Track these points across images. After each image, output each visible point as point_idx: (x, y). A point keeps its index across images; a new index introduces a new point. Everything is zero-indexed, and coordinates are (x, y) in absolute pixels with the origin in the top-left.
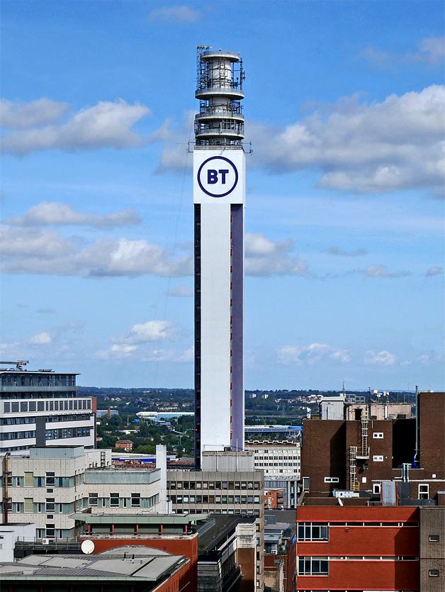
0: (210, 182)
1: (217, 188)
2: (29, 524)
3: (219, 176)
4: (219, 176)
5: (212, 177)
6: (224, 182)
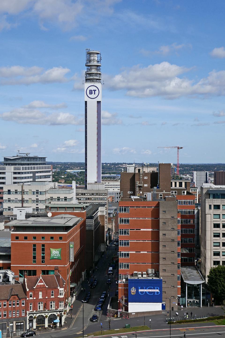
0: (90, 94)
1: (92, 96)
2: (30, 207)
3: (93, 92)
4: (93, 92)
5: (91, 92)
6: (95, 94)
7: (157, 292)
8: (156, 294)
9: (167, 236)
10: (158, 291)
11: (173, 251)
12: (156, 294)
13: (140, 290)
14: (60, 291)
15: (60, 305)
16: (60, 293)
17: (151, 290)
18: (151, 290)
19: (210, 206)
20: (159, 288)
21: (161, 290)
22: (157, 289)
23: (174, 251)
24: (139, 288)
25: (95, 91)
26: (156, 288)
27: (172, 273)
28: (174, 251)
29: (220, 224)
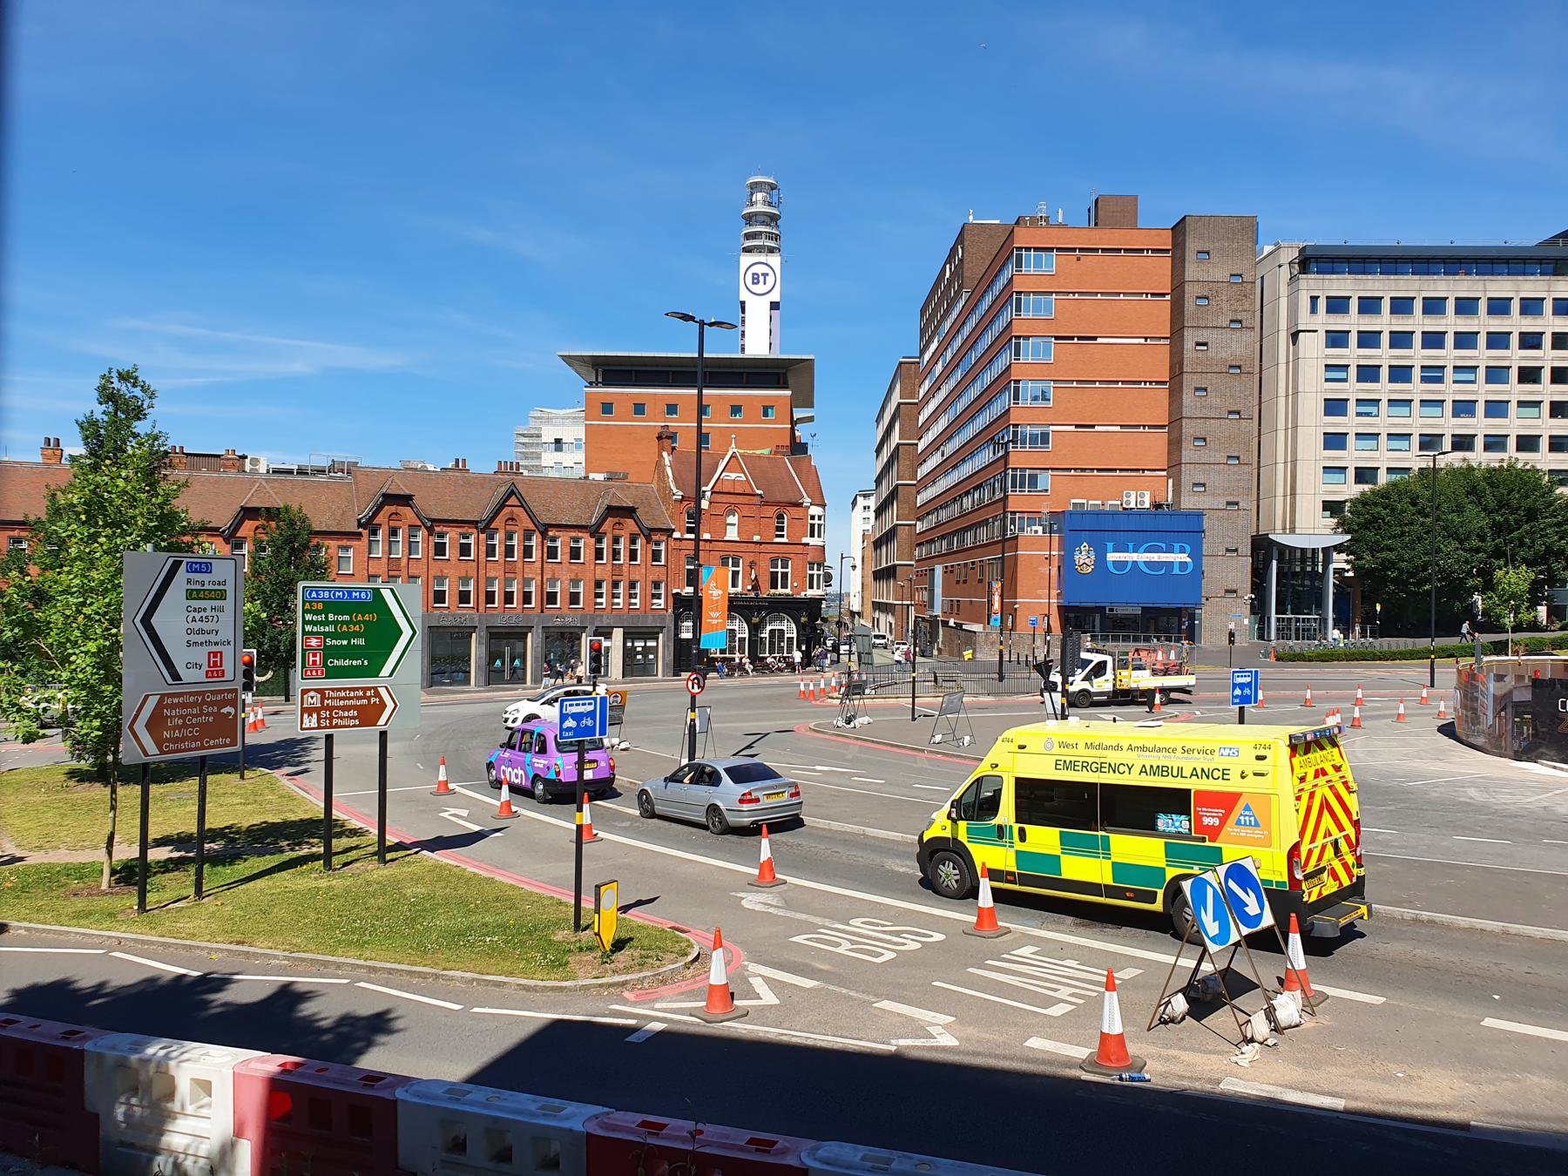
7: (1183, 565)
8: (1176, 571)
9: (1212, 353)
10: (1184, 557)
11: (1235, 408)
12: (1176, 571)
13: (1112, 557)
14: (813, 518)
15: (812, 576)
16: (812, 526)
17: (1155, 557)
18: (1155, 557)
19: (1314, 299)
20: (1188, 548)
21: (1196, 555)
22: (1182, 551)
23: (1238, 413)
24: (1110, 545)
25: (765, 275)
26: (1177, 546)
27: (1231, 499)
28: (1238, 413)
29: (1360, 346)
